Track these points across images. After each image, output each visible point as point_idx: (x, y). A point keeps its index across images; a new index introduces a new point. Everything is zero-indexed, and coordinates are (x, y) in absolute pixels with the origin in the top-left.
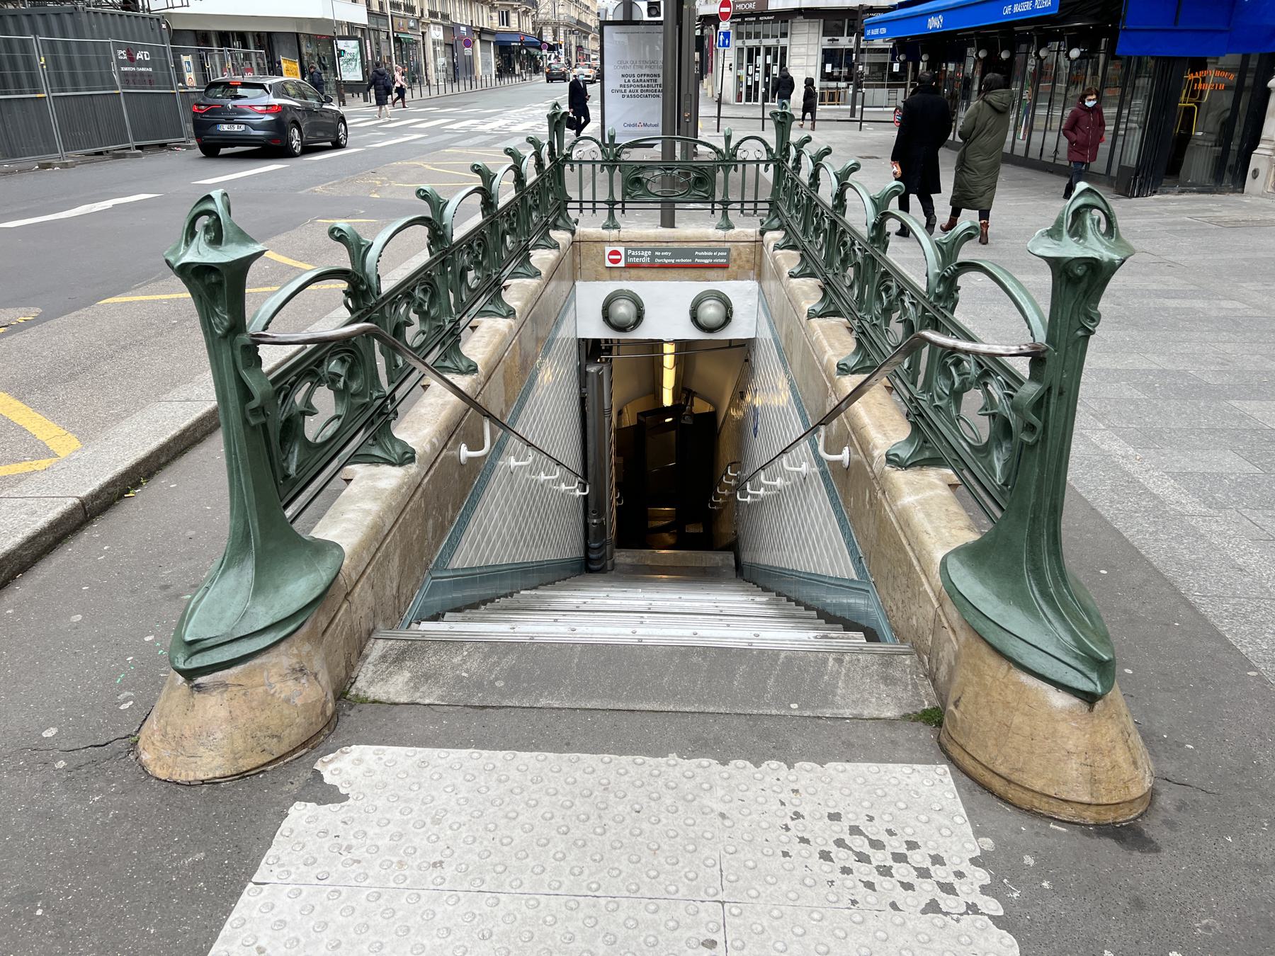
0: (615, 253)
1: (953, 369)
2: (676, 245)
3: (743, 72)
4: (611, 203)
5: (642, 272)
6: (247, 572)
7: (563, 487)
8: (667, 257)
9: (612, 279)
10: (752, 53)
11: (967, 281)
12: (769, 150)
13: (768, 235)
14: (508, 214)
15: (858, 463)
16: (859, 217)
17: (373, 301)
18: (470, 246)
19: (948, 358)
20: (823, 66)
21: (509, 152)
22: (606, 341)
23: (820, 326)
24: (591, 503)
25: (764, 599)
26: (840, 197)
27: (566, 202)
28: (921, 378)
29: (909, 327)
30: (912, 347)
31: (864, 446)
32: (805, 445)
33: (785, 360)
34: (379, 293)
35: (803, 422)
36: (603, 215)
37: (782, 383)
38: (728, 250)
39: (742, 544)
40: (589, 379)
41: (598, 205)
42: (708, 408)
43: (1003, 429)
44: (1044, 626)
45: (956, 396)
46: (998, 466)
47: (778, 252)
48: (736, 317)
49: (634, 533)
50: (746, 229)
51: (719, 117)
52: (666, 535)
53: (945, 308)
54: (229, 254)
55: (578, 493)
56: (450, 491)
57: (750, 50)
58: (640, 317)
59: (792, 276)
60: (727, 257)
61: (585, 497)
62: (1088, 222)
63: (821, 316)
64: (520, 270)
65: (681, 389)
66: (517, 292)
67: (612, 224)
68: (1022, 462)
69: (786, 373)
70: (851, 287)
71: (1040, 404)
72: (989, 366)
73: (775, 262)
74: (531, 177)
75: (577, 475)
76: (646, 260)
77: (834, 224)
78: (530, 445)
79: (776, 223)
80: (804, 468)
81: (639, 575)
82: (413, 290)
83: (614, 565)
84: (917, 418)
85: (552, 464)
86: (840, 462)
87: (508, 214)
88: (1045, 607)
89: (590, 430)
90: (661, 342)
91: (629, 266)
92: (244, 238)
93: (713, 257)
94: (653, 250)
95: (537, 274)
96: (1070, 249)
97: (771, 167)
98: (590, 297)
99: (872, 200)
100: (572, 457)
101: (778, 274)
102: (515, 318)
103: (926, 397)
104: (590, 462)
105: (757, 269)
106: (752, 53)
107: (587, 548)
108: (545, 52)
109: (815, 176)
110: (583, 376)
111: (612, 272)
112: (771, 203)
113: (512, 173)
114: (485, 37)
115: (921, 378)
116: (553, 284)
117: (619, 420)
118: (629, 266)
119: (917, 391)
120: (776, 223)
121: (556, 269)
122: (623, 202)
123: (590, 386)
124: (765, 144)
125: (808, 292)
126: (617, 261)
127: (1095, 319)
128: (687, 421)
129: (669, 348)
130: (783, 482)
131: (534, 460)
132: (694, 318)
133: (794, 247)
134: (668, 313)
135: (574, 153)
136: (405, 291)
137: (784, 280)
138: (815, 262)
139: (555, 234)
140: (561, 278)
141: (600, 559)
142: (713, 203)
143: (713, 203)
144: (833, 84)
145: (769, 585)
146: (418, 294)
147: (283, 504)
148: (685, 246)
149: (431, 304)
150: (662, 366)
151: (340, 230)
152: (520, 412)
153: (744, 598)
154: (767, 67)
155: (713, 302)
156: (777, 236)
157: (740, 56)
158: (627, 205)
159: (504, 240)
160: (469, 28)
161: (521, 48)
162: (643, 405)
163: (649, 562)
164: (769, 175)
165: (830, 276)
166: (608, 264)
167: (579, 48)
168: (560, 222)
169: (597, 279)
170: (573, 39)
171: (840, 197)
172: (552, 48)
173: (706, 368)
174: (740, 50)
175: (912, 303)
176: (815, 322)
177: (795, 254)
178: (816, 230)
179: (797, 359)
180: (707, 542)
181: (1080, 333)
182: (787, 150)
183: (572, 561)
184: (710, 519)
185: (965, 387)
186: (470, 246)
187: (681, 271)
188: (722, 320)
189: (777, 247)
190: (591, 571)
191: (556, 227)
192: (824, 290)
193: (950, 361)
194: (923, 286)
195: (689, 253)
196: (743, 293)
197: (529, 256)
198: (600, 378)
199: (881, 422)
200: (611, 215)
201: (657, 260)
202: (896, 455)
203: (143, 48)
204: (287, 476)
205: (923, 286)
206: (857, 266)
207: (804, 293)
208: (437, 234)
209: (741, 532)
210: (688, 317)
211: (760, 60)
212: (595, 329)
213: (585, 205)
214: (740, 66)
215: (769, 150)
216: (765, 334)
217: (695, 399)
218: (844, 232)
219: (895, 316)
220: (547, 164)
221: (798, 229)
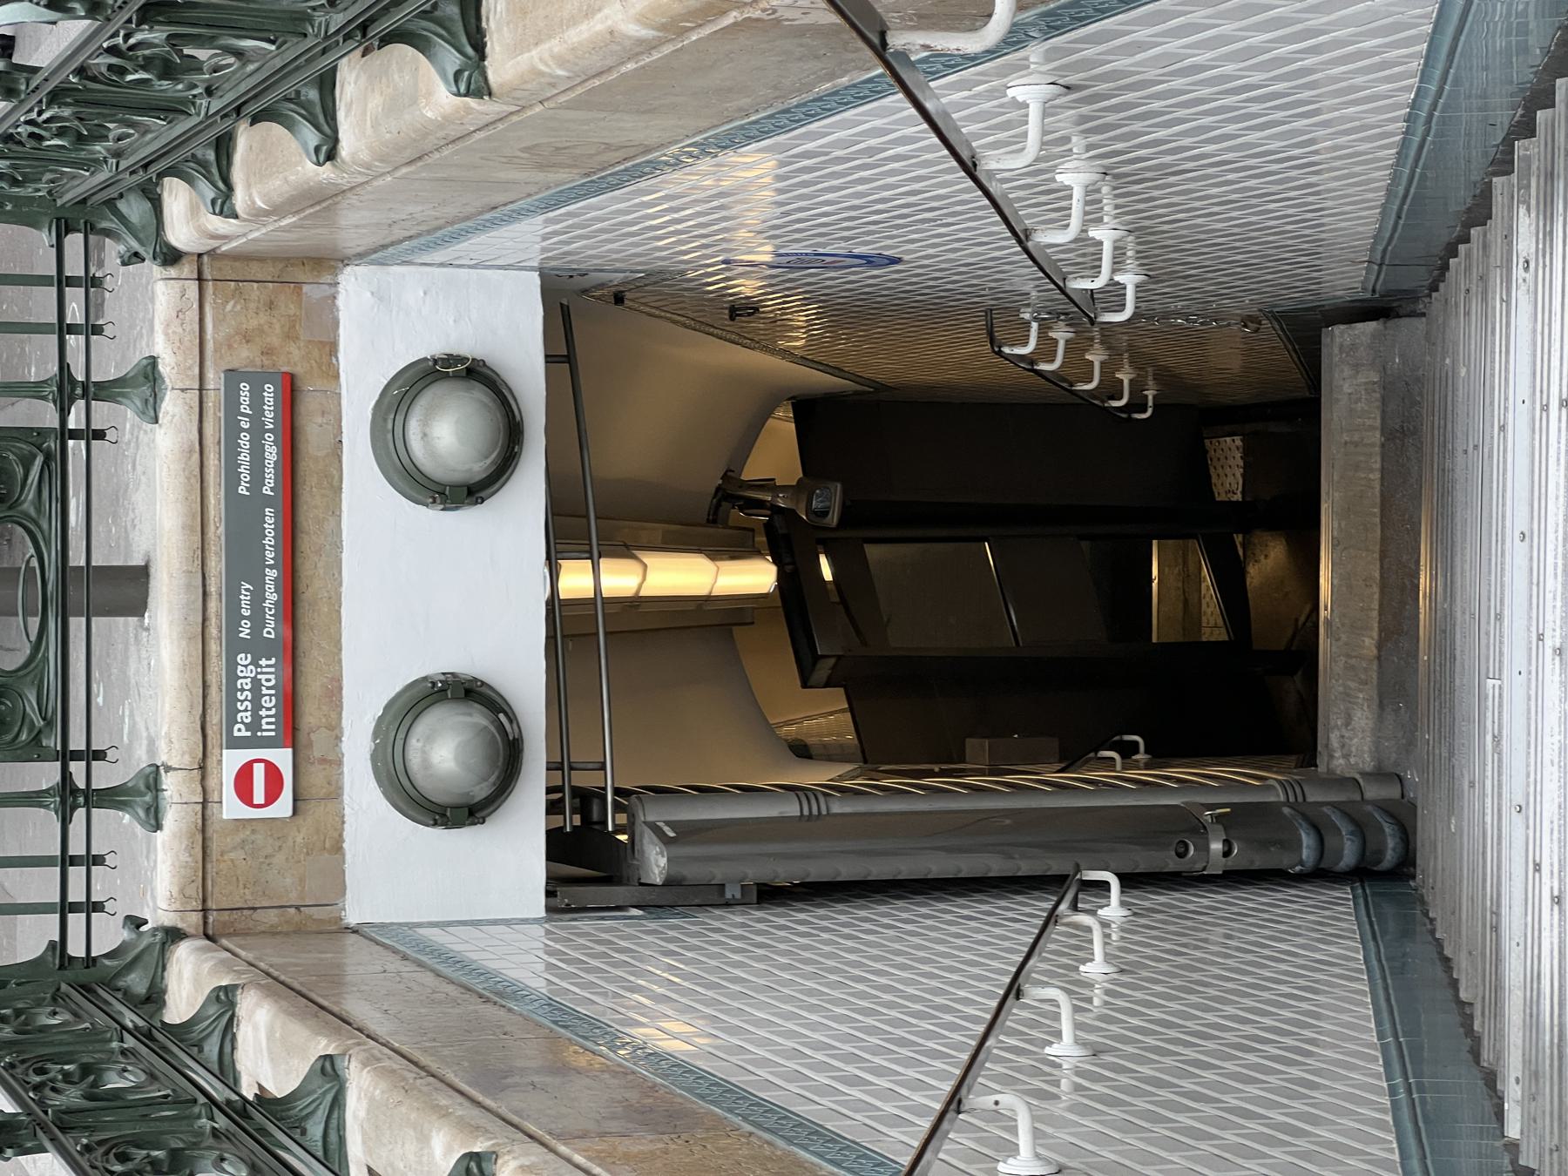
0: (244, 779)
2: (217, 565)
4: (68, 798)
5: (312, 686)
7: (1096, 969)
8: (258, 597)
9: (335, 793)
13: (179, 233)
14: (37, 1088)
22: (553, 808)
23: (519, 47)
24: (1144, 860)
25: (1525, 226)
27: (66, 961)
32: (943, 94)
33: (634, 167)
35: (862, 100)
36: (112, 828)
37: (701, 177)
38: (233, 377)
39: (1290, 299)
40: (693, 872)
41: (77, 848)
42: (783, 427)
47: (240, 200)
48: (467, 344)
49: (1251, 697)
50: (153, 316)
51: (205, 910)
52: (1255, 574)
55: (1114, 909)
58: (467, 691)
59: (329, 152)
60: (257, 381)
61: (1130, 881)
63: (480, 49)
64: (315, 1130)
65: (716, 524)
67: (143, 798)
69: (677, 164)
73: (277, 211)
75: (1051, 918)
76: (269, 672)
78: (954, 1102)
79: (134, 209)
80: (1029, 91)
81: (1421, 673)
83: (1381, 774)
85: (1016, 1013)
87: (37, 1088)
89: (879, 869)
90: (555, 606)
91: (291, 732)
93: (257, 431)
94: (234, 646)
95: (328, 1069)
98: (396, 872)
100: (986, 936)
101: (320, 201)
102: (493, 1156)
104: (995, 866)
105: (293, 272)
107: (1321, 875)
110: (682, 897)
111: (314, 793)
112: (64, 227)
116: (356, 1008)
117: (830, 755)
118: (291, 732)
120: (134, 209)
121: (310, 1000)
122: (66, 756)
123: (718, 873)
125: (389, 97)
126: (273, 774)
128: (831, 501)
129: (576, 580)
131: (1007, 1081)
132: (468, 493)
133: (224, 146)
134: (449, 591)
137: (344, 180)
138: (283, 73)
139: (181, 1004)
140: (335, 978)
141: (1361, 828)
142: (65, 434)
143: (65, 434)
145: (1461, 198)
148: (217, 530)
150: (634, 604)
152: (833, 1139)
153: (1521, 297)
155: (414, 427)
156: (178, 198)
158: (77, 743)
159: (117, 1094)
162: (771, 663)
163: (1369, 643)
165: (216, 105)
166: (283, 807)
168: (137, 982)
169: (338, 848)
173: (643, 439)
176: (501, 67)
177: (246, 139)
178: (168, 70)
179: (631, 129)
180: (1285, 423)
183: (1373, 934)
184: (1191, 417)
187: (306, 544)
188: (479, 393)
189: (223, 205)
190: (1405, 868)
191: (154, 998)
192: (386, 40)
195: (242, 515)
196: (381, 324)
197: (264, 1100)
198: (687, 833)
200: (112, 798)
201: (269, 632)
207: (395, 106)
209: (1248, 303)
210: (467, 520)
212: (515, 848)
213: (76, 894)
216: (529, 239)
217: (747, 475)
221: (159, 132)
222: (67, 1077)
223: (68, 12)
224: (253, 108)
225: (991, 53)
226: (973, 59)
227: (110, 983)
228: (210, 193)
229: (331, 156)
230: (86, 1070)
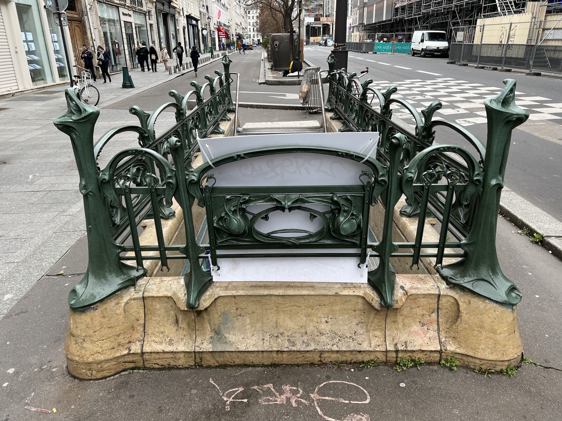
12: (481, 157)
18: (193, 118)
21: (207, 78)
34: (155, 138)
70: (354, 119)
74: (218, 89)
77: (347, 96)
99: (361, 85)
113: (209, 87)
147: (114, 238)
197: (219, 124)
202: (405, 212)
204: (114, 224)
208: (180, 115)
215: (481, 157)
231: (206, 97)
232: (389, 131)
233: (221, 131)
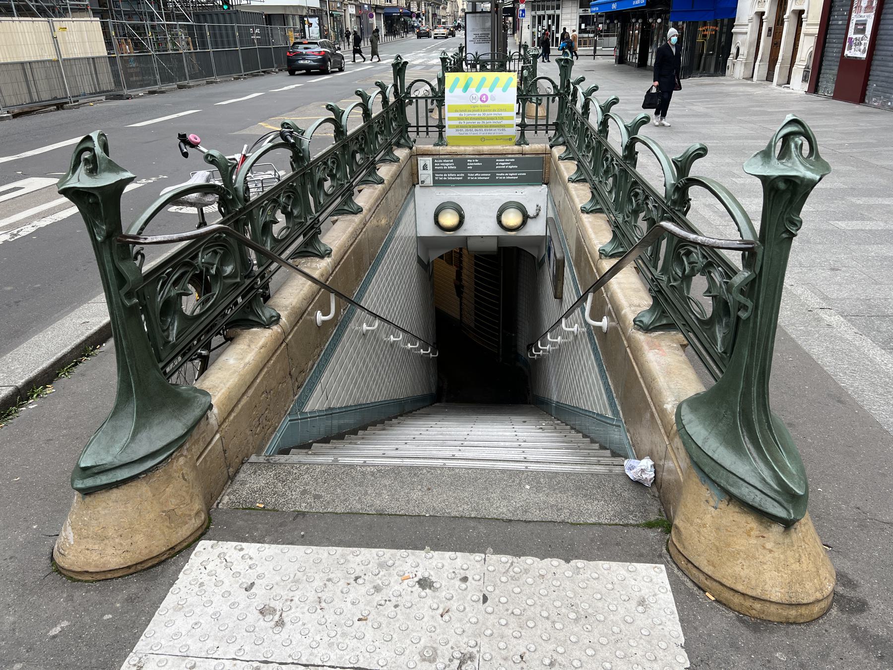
1: (685, 259)
3: (535, 30)
6: (129, 425)
10: (541, 19)
11: (694, 192)
12: (555, 87)
15: (615, 328)
16: (617, 139)
17: (240, 206)
19: (681, 247)
20: (580, 26)
26: (604, 124)
28: (660, 263)
29: (652, 222)
30: (656, 234)
31: (616, 314)
43: (722, 307)
44: (751, 464)
45: (687, 279)
46: (719, 337)
53: (679, 211)
54: (107, 179)
56: (306, 350)
57: (539, 17)
62: (793, 145)
66: (365, 197)
68: (737, 323)
70: (610, 192)
71: (751, 288)
72: (711, 257)
82: (279, 197)
84: (658, 294)
86: (600, 327)
88: (755, 455)
92: (113, 167)
96: (776, 169)
97: (557, 98)
103: (665, 278)
106: (541, 19)
108: (414, 19)
109: (586, 107)
113: (380, 96)
114: (379, 11)
115: (660, 263)
119: (657, 273)
120: (561, 139)
124: (552, 83)
125: (581, 194)
127: (798, 224)
130: (564, 334)
135: (412, 91)
136: (272, 198)
144: (586, 35)
146: (282, 200)
149: (294, 206)
151: (212, 156)
154: (549, 26)
156: (563, 148)
157: (534, 21)
160: (369, 5)
161: (400, 17)
164: (555, 107)
165: (596, 183)
167: (434, 15)
170: (430, 8)
171: (604, 124)
172: (418, 16)
174: (534, 17)
175: (654, 206)
178: (588, 146)
181: (784, 236)
182: (568, 86)
185: (693, 273)
186: (325, 163)
191: (399, 145)
193: (682, 252)
194: (661, 192)
199: (629, 292)
202: (641, 321)
203: (257, 27)
204: (167, 342)
205: (661, 192)
206: (614, 176)
211: (545, 22)
214: (534, 26)
215: (555, 87)
218: (606, 150)
219: (642, 215)
220: (392, 99)
221: (575, 145)
222: (361, 145)
223: (624, 151)
224: (617, 232)
225: (585, 321)
226: (584, 316)
227: (402, 136)
228: (588, 207)
229: (583, 211)
230: (383, 132)
231: (376, 109)
232: (632, 186)
233: (323, 249)
